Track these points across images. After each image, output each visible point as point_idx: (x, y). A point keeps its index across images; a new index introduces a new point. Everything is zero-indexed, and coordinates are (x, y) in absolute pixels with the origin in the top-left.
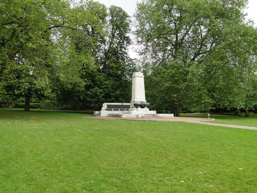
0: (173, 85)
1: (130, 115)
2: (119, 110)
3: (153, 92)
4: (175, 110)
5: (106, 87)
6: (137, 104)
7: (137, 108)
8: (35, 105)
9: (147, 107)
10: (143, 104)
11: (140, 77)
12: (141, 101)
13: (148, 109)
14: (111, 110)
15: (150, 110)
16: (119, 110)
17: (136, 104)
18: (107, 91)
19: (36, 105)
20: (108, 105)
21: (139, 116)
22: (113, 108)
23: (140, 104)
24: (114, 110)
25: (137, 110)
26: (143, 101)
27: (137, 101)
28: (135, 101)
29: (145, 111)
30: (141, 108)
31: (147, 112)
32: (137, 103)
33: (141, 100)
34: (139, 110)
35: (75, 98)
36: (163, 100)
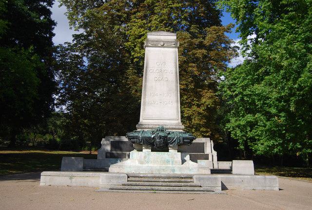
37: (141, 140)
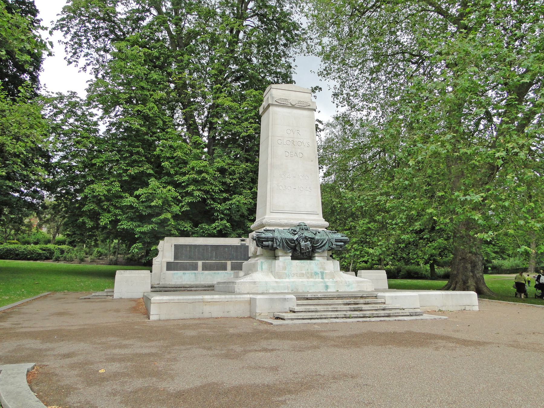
0: (462, 151)
1: (204, 302)
2: (229, 267)
3: (374, 197)
4: (469, 266)
5: (195, 182)
6: (272, 239)
7: (275, 257)
8: (40, 251)
9: (326, 254)
10: (306, 239)
11: (293, 106)
12: (297, 222)
13: (333, 265)
14: (194, 267)
15: (345, 268)
16: (229, 267)
17: (267, 239)
18: (197, 193)
19: (44, 250)
20: (176, 246)
21: (258, 311)
22: (200, 260)
23: (291, 236)
24: (206, 268)
25: (271, 270)
26: (307, 222)
27: (273, 221)
28: (264, 221)
29: (316, 274)
30: (294, 258)
31: (329, 281)
32: (270, 235)
33: (296, 219)
34: (285, 268)
35: (84, 223)
36: (417, 226)
37: (278, 243)
